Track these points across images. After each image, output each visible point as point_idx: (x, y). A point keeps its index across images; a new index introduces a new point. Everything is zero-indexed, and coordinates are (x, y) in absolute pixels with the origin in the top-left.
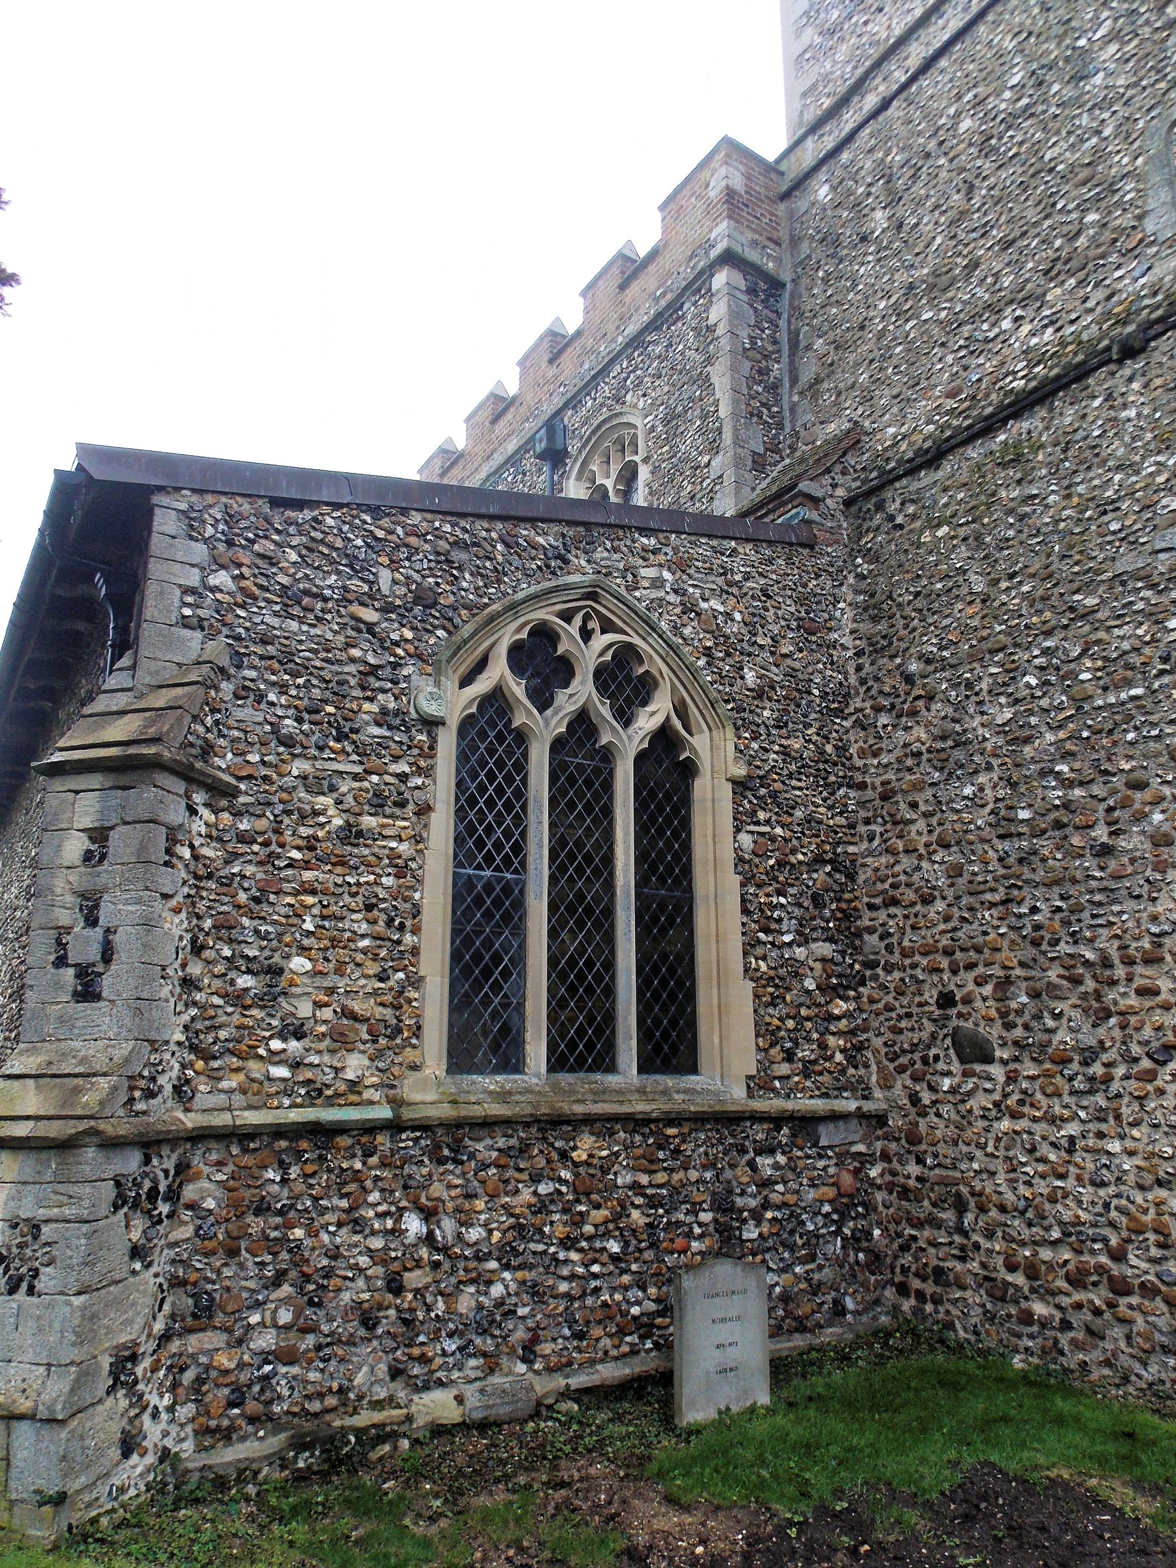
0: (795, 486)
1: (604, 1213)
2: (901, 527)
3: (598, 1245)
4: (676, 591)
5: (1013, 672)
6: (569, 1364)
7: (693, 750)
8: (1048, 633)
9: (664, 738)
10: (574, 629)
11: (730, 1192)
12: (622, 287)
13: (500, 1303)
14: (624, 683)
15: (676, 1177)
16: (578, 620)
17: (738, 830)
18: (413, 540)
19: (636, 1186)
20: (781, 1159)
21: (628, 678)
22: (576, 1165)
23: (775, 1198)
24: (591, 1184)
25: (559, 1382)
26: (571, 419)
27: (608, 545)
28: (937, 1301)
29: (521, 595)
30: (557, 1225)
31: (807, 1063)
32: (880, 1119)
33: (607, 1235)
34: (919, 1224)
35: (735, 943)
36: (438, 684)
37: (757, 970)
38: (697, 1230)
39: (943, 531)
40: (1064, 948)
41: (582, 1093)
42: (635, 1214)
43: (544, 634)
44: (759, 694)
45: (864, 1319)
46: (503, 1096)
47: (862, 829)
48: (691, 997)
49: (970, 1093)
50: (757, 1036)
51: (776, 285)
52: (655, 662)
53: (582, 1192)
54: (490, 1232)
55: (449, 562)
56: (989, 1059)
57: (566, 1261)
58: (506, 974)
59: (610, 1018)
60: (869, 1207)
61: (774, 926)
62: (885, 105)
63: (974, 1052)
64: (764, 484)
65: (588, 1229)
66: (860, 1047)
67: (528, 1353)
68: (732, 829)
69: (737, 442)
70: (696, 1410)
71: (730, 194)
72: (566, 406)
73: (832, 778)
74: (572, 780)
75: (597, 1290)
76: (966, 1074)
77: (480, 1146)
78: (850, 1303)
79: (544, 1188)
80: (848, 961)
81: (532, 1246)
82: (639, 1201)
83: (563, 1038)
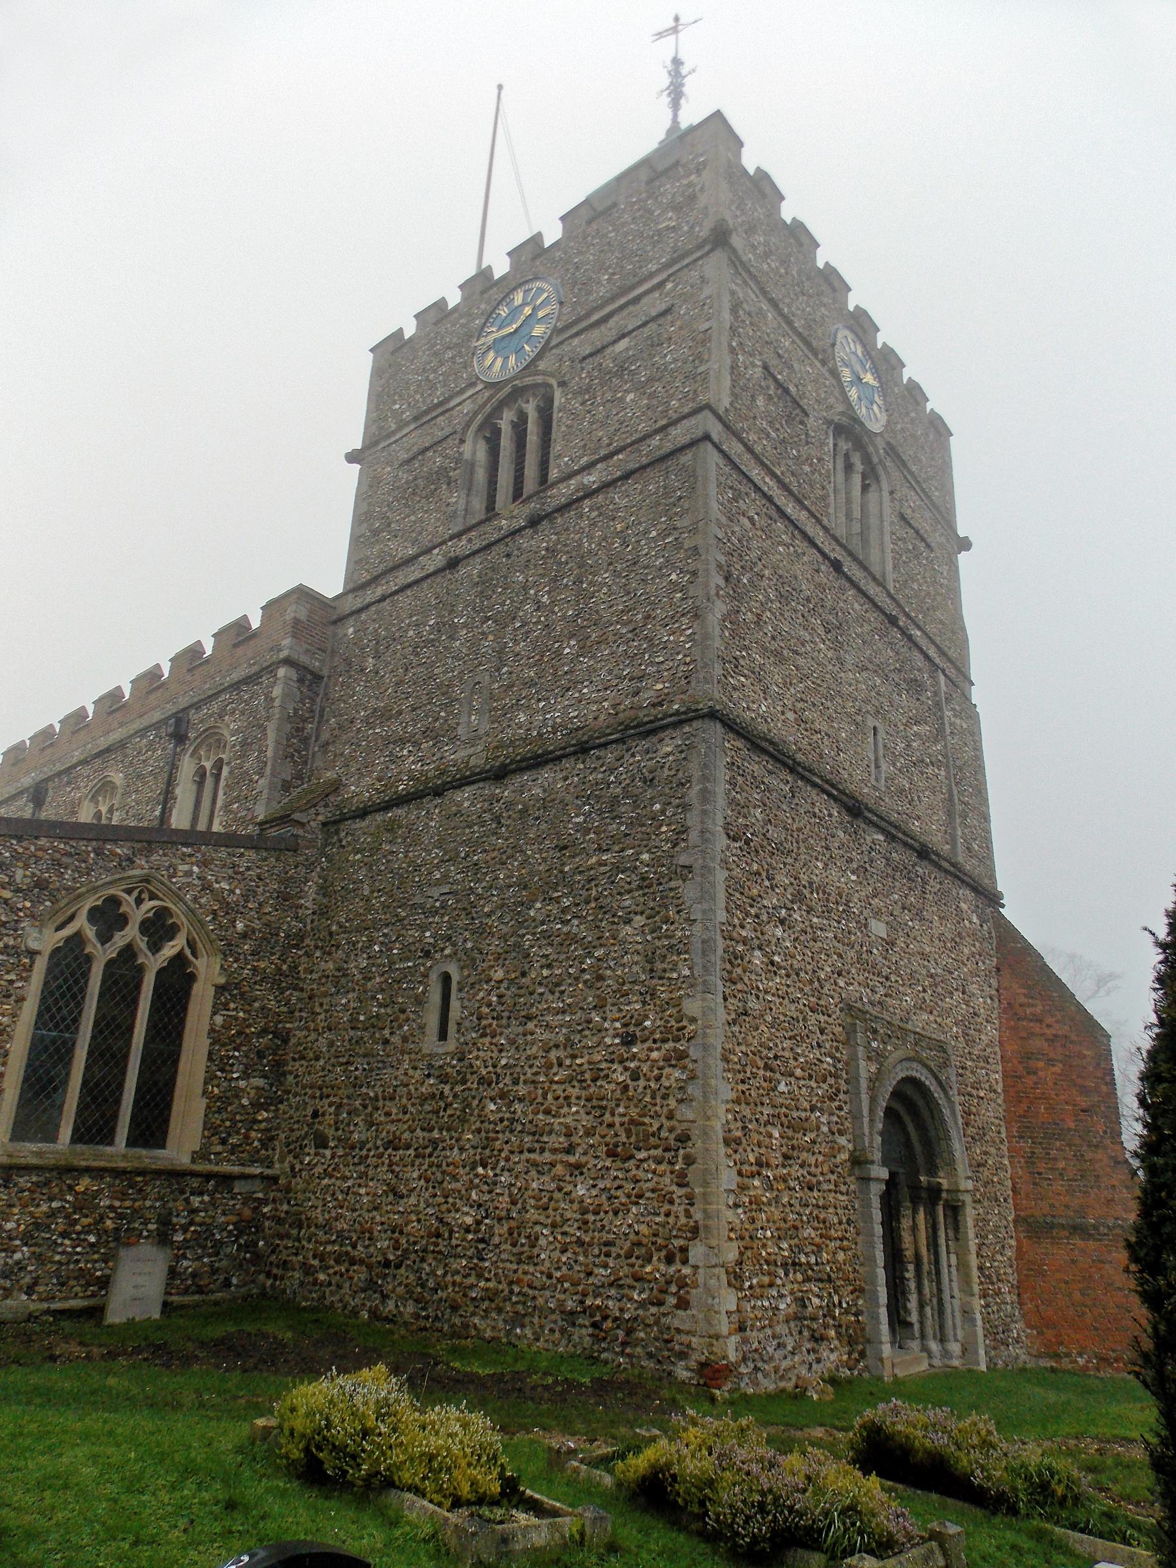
0: (289, 815)
1: (89, 1220)
2: (343, 847)
3: (82, 1237)
4: (199, 878)
5: (371, 941)
6: (53, 1298)
7: (195, 967)
8: (387, 925)
9: (179, 960)
10: (131, 899)
11: (170, 1214)
12: (236, 646)
13: (18, 1263)
14: (158, 928)
15: (137, 1204)
16: (135, 893)
17: (214, 1013)
18: (40, 854)
19: (111, 1208)
20: (206, 1198)
21: (163, 925)
22: (77, 1193)
23: (197, 1219)
24: (84, 1204)
25: (45, 1305)
26: (194, 716)
27: (161, 852)
28: (282, 1279)
29: (100, 883)
30: (60, 1223)
31: (234, 1146)
32: (274, 1179)
33: (89, 1233)
34: (281, 1237)
35: (201, 1076)
36: (40, 932)
37: (212, 1092)
38: (145, 1233)
39: (359, 856)
40: (364, 1090)
41: (88, 1155)
42: (109, 1223)
43: (114, 901)
44: (244, 936)
45: (242, 1290)
46: (39, 1154)
47: (297, 1014)
48: (169, 1106)
49: (316, 1164)
50: (204, 1129)
51: (318, 678)
52: (179, 916)
53: (78, 1208)
54: (19, 1225)
55: (60, 865)
56: (326, 1147)
57: (62, 1244)
58: (55, 1089)
59: (115, 1116)
60: (259, 1229)
61: (228, 1068)
62: (383, 599)
63: (321, 1142)
64: (286, 800)
65: (78, 1228)
66: (272, 1139)
67: (30, 1290)
68: (210, 1013)
69: (273, 774)
70: (116, 1315)
71: (296, 622)
72: (191, 706)
73: (284, 984)
74: (116, 982)
75: (78, 1261)
76: (316, 1154)
77: (21, 1180)
78: (234, 1281)
79: (54, 1205)
80: (274, 1089)
81: (43, 1234)
82: (112, 1215)
83: (84, 1125)
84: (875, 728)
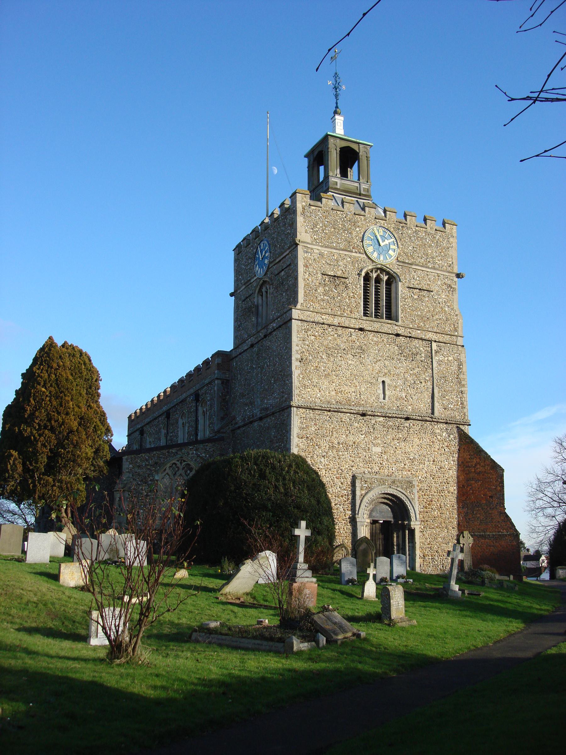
71: (218, 364)
84: (383, 382)
